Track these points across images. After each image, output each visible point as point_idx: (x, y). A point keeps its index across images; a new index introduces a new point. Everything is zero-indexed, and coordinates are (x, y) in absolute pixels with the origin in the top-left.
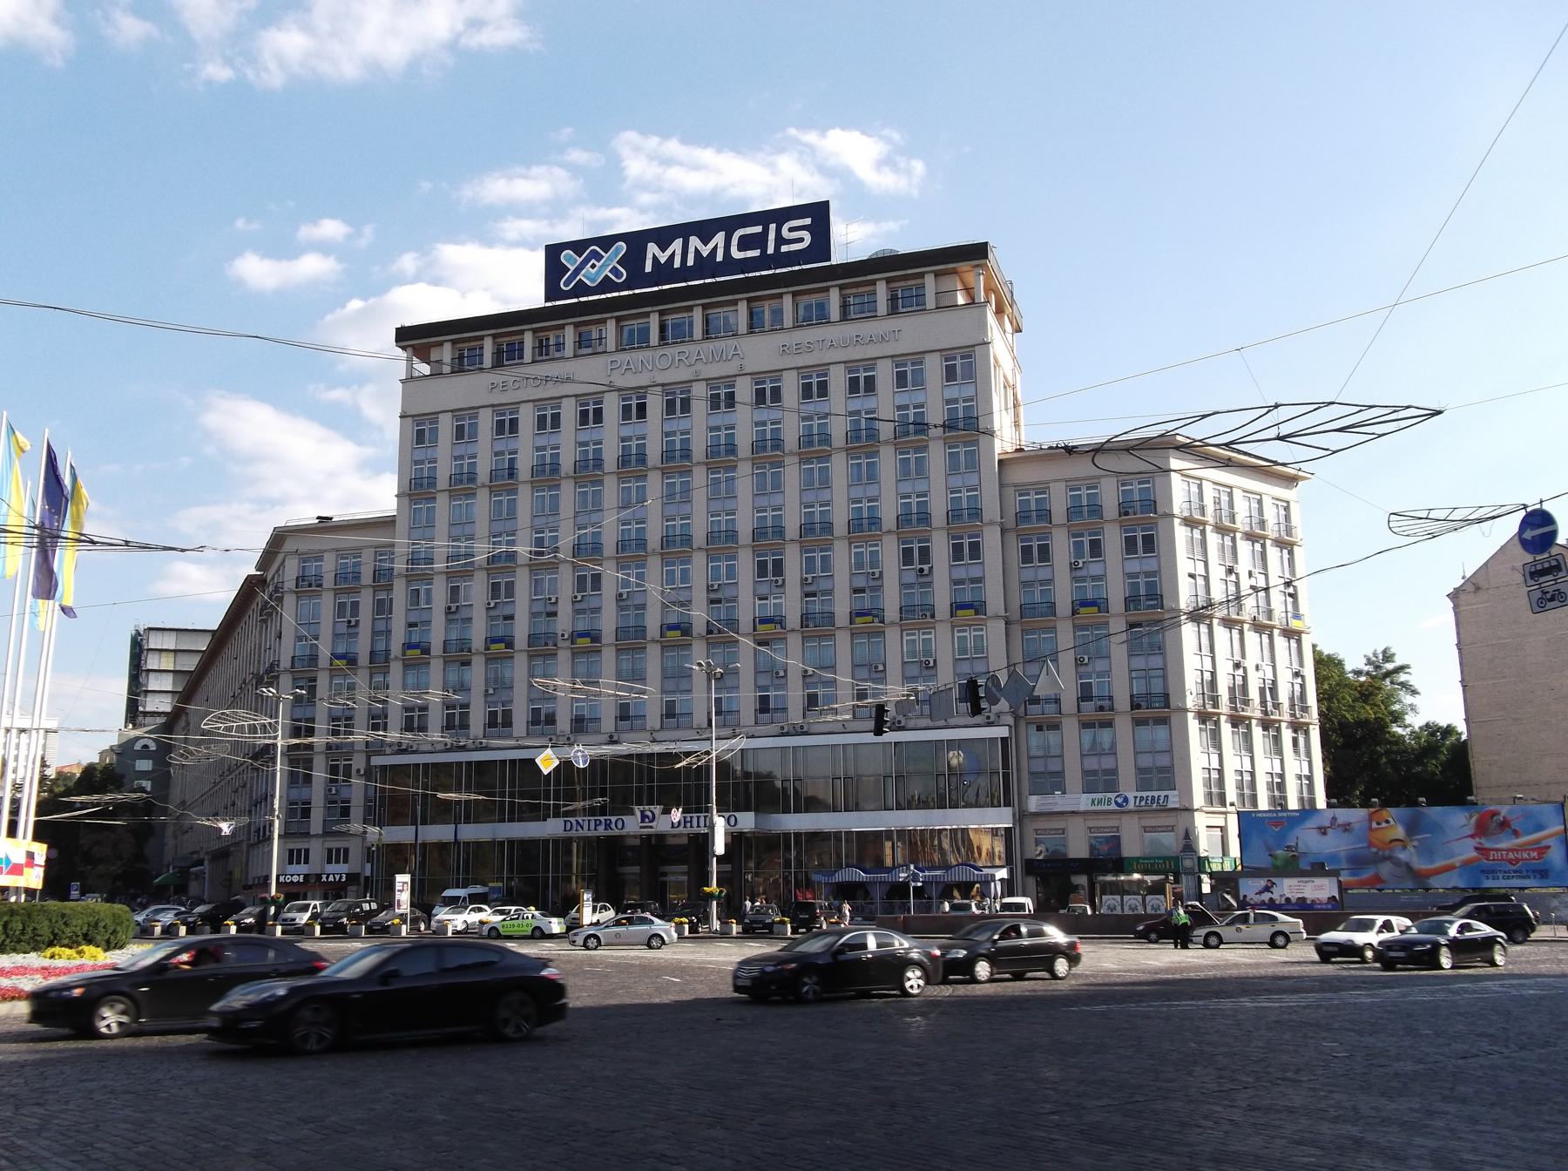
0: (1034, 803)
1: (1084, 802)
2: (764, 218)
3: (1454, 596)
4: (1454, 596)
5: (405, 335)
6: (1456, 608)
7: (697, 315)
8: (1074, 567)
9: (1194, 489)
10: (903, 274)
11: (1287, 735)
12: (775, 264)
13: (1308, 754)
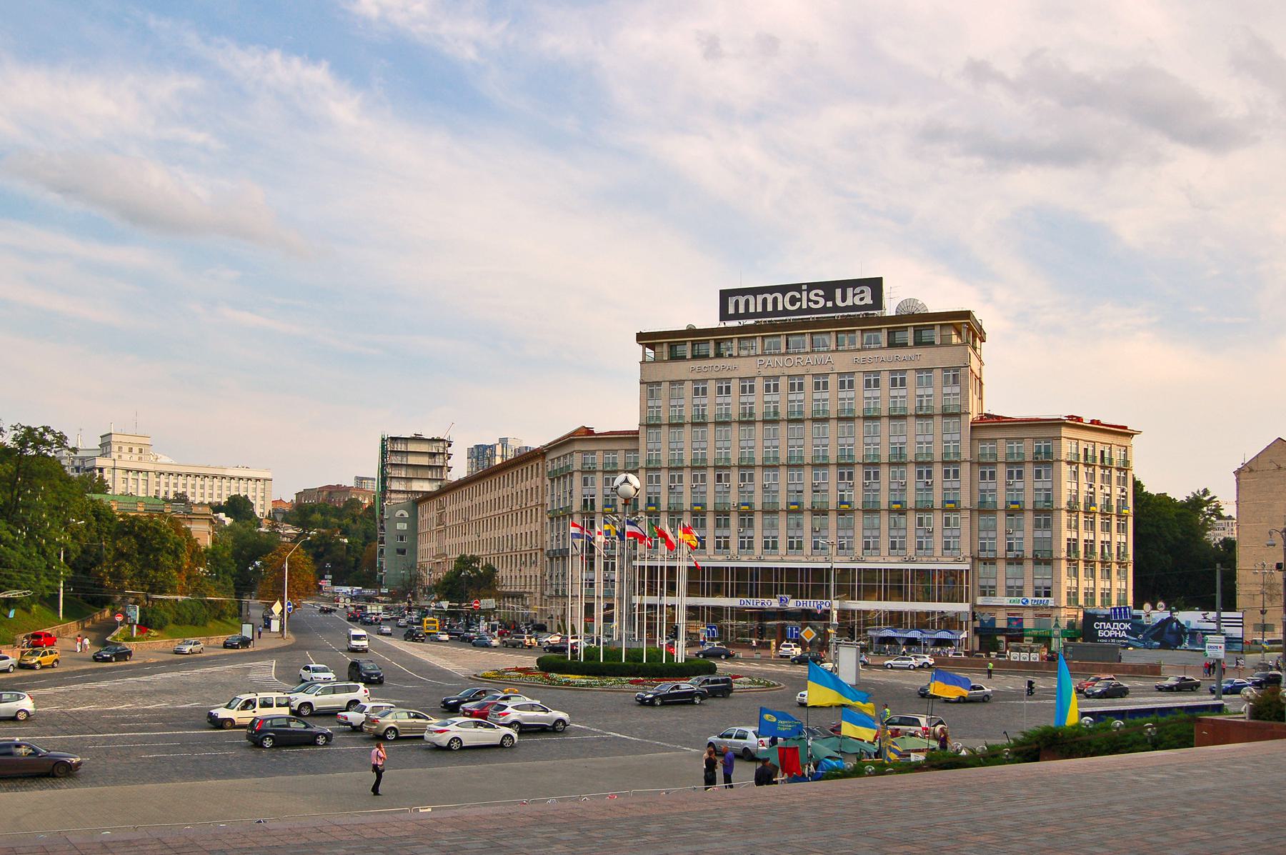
0: (980, 600)
1: (1006, 601)
2: (797, 287)
3: (1238, 473)
4: (1238, 473)
5: (641, 337)
6: (1238, 480)
7: (783, 339)
8: (1008, 484)
9: (1074, 446)
10: (920, 326)
11: (1115, 567)
12: (846, 310)
13: (1126, 578)
